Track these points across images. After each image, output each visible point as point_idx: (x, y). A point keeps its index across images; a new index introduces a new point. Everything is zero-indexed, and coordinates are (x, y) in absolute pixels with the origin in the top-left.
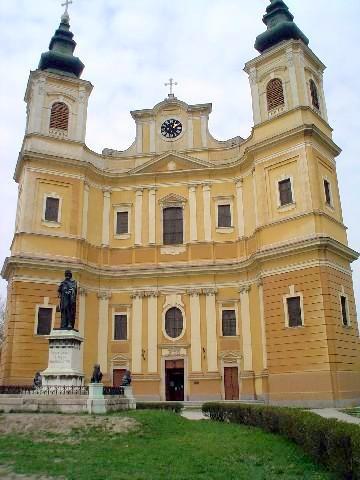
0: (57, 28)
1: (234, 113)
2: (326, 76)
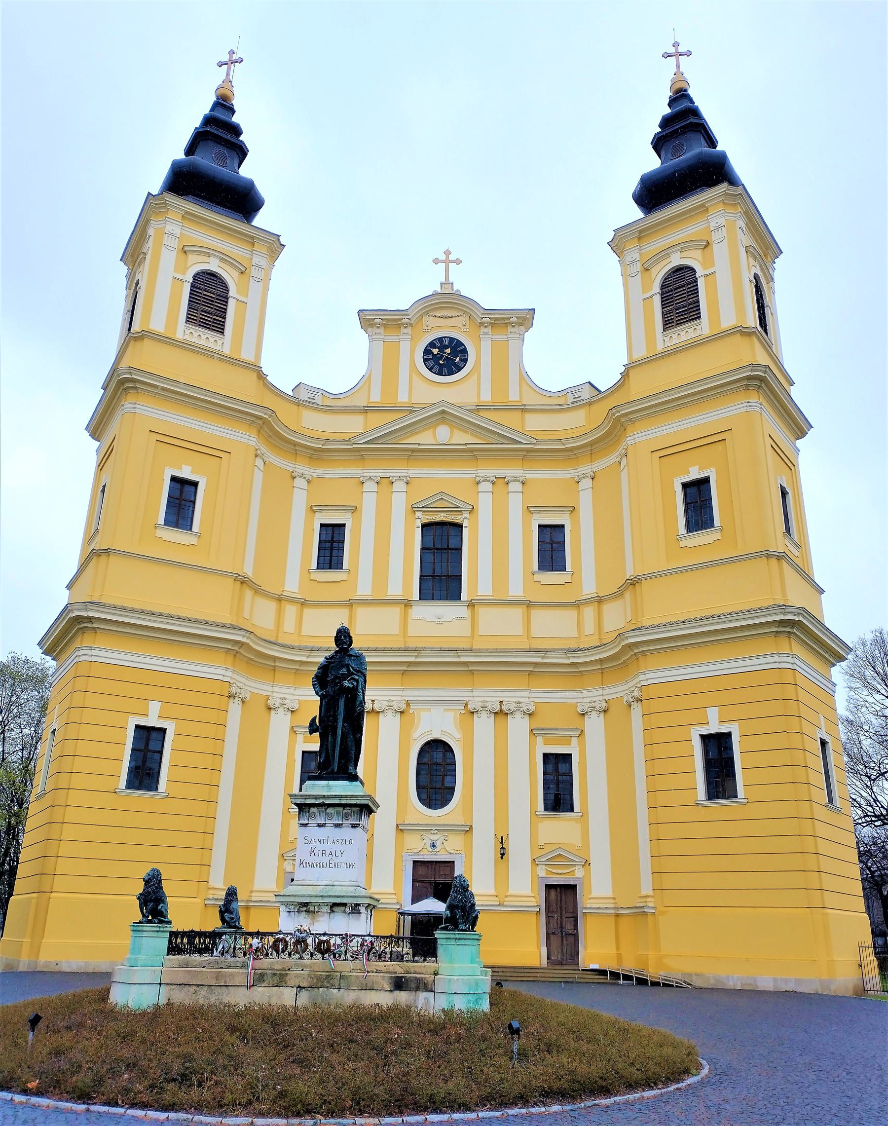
0: (206, 110)
1: (582, 332)
2: (781, 267)
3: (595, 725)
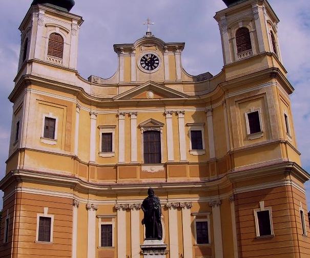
3: (216, 210)
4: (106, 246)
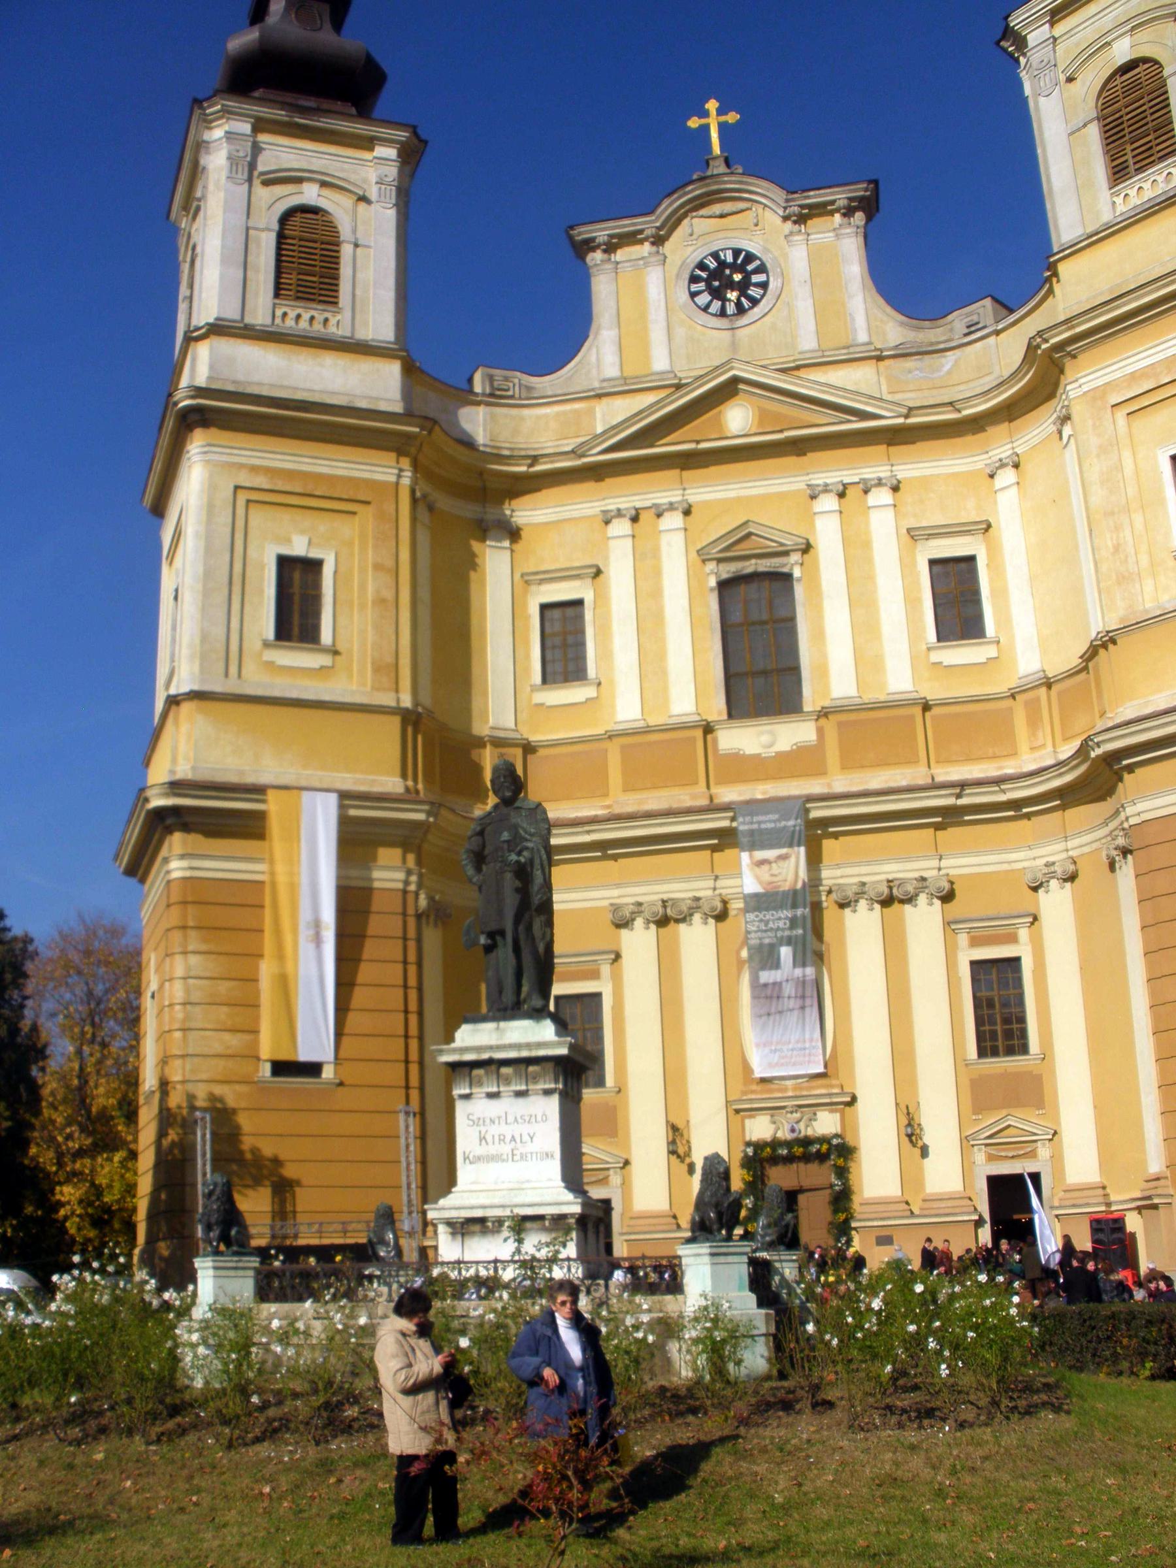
4: (995, 1053)
